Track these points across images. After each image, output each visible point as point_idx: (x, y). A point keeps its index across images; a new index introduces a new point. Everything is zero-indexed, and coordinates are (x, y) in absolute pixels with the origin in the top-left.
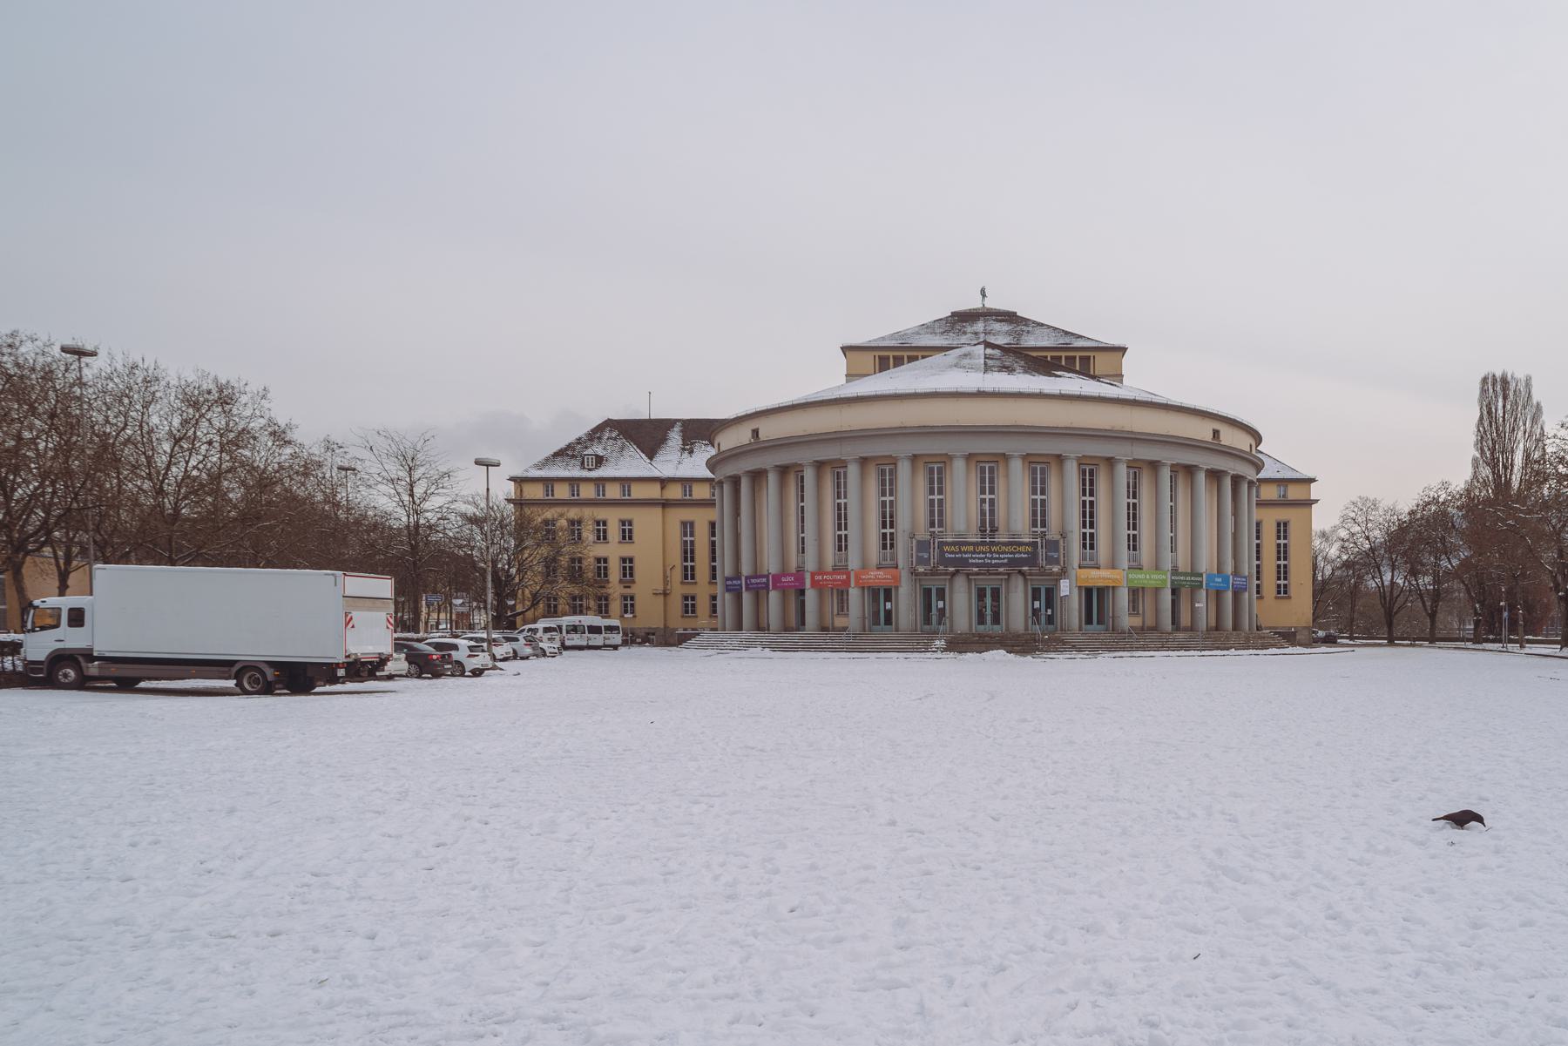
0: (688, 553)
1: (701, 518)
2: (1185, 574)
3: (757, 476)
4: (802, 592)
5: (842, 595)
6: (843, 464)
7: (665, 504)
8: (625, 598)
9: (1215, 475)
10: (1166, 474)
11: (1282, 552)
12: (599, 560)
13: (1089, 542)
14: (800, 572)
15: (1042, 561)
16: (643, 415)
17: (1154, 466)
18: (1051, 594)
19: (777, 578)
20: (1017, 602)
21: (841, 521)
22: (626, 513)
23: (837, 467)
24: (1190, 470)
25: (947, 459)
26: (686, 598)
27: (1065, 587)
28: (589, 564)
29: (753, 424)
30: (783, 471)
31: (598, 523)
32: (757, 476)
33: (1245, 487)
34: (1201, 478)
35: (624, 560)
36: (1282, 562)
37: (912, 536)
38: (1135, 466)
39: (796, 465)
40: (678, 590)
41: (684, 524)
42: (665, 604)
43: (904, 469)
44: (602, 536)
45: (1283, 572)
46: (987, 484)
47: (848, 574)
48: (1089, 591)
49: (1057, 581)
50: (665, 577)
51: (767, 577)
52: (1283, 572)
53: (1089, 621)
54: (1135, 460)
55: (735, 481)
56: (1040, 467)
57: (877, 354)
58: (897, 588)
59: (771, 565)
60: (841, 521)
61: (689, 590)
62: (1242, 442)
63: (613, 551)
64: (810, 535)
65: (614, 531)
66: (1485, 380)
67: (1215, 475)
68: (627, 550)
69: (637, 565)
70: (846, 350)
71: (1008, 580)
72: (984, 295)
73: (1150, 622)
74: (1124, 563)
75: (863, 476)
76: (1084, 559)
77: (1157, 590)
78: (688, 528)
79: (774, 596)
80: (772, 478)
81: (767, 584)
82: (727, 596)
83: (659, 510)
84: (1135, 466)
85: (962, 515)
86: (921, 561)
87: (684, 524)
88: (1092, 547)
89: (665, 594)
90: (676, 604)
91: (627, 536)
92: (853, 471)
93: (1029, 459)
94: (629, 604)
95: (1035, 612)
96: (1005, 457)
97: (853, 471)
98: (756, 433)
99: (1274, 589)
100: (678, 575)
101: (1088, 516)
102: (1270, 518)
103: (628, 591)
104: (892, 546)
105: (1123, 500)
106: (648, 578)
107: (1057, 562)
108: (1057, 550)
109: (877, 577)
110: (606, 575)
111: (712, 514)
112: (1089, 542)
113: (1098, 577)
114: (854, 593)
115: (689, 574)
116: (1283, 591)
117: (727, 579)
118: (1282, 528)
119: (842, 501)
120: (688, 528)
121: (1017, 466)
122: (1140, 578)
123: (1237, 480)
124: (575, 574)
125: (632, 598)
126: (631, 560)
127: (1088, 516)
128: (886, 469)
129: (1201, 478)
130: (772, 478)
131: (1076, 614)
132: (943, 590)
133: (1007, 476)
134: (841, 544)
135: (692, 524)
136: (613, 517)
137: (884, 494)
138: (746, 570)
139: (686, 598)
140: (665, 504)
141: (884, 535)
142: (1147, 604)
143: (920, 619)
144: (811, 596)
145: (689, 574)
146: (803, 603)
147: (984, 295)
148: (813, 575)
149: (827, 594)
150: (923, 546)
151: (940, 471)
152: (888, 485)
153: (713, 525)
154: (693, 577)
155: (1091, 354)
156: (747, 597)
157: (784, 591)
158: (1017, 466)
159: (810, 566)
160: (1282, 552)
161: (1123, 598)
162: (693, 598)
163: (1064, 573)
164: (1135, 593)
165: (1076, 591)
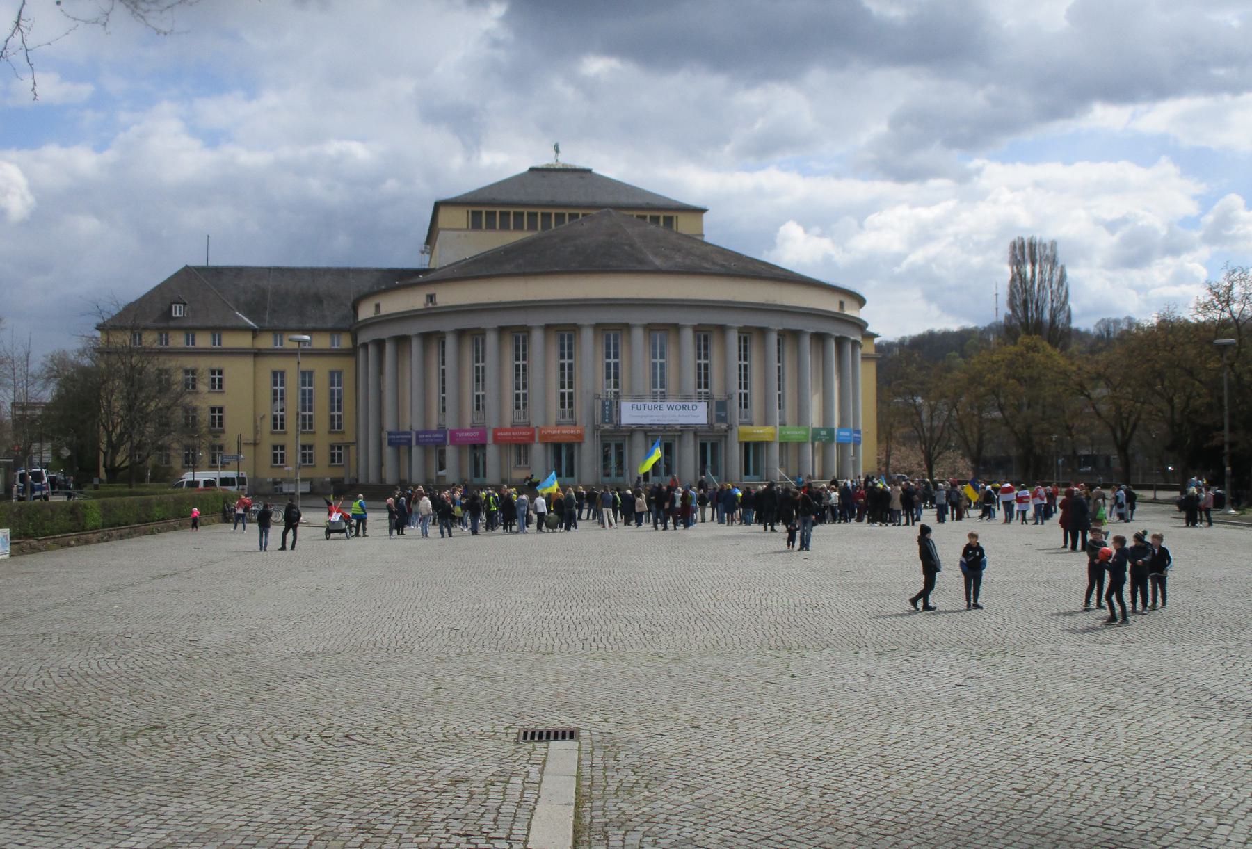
3: (402, 342)
7: (257, 354)
9: (820, 338)
10: (773, 338)
12: (213, 410)
13: (745, 401)
17: (763, 332)
19: (453, 433)
22: (216, 363)
23: (478, 335)
24: (796, 334)
25: (575, 329)
26: (275, 448)
28: (204, 416)
29: (430, 290)
30: (426, 337)
31: (213, 372)
32: (402, 342)
33: (849, 346)
34: (806, 342)
38: (746, 335)
39: (437, 333)
40: (268, 441)
41: (275, 374)
46: (612, 351)
48: (747, 445)
50: (256, 427)
53: (747, 473)
54: (745, 327)
56: (704, 335)
57: (471, 209)
58: (580, 444)
59: (413, 422)
61: (279, 440)
62: (829, 304)
63: (205, 400)
66: (1013, 246)
68: (216, 400)
71: (680, 436)
75: (500, 340)
76: (563, 416)
78: (278, 376)
80: (416, 345)
81: (410, 440)
84: (783, 334)
88: (746, 406)
90: (266, 452)
91: (217, 384)
92: (491, 339)
96: (627, 327)
97: (491, 339)
98: (431, 298)
100: (267, 425)
105: (734, 361)
106: (238, 425)
110: (221, 425)
113: (760, 432)
119: (480, 364)
120: (278, 376)
121: (688, 337)
123: (840, 342)
126: (221, 410)
128: (520, 335)
129: (806, 342)
130: (416, 345)
131: (738, 466)
133: (630, 343)
135: (282, 374)
136: (204, 364)
137: (517, 359)
138: (389, 426)
139: (275, 448)
140: (257, 354)
143: (600, 471)
144: (492, 452)
151: (570, 339)
152: (522, 351)
155: (674, 214)
158: (638, 335)
161: (775, 451)
164: (783, 445)
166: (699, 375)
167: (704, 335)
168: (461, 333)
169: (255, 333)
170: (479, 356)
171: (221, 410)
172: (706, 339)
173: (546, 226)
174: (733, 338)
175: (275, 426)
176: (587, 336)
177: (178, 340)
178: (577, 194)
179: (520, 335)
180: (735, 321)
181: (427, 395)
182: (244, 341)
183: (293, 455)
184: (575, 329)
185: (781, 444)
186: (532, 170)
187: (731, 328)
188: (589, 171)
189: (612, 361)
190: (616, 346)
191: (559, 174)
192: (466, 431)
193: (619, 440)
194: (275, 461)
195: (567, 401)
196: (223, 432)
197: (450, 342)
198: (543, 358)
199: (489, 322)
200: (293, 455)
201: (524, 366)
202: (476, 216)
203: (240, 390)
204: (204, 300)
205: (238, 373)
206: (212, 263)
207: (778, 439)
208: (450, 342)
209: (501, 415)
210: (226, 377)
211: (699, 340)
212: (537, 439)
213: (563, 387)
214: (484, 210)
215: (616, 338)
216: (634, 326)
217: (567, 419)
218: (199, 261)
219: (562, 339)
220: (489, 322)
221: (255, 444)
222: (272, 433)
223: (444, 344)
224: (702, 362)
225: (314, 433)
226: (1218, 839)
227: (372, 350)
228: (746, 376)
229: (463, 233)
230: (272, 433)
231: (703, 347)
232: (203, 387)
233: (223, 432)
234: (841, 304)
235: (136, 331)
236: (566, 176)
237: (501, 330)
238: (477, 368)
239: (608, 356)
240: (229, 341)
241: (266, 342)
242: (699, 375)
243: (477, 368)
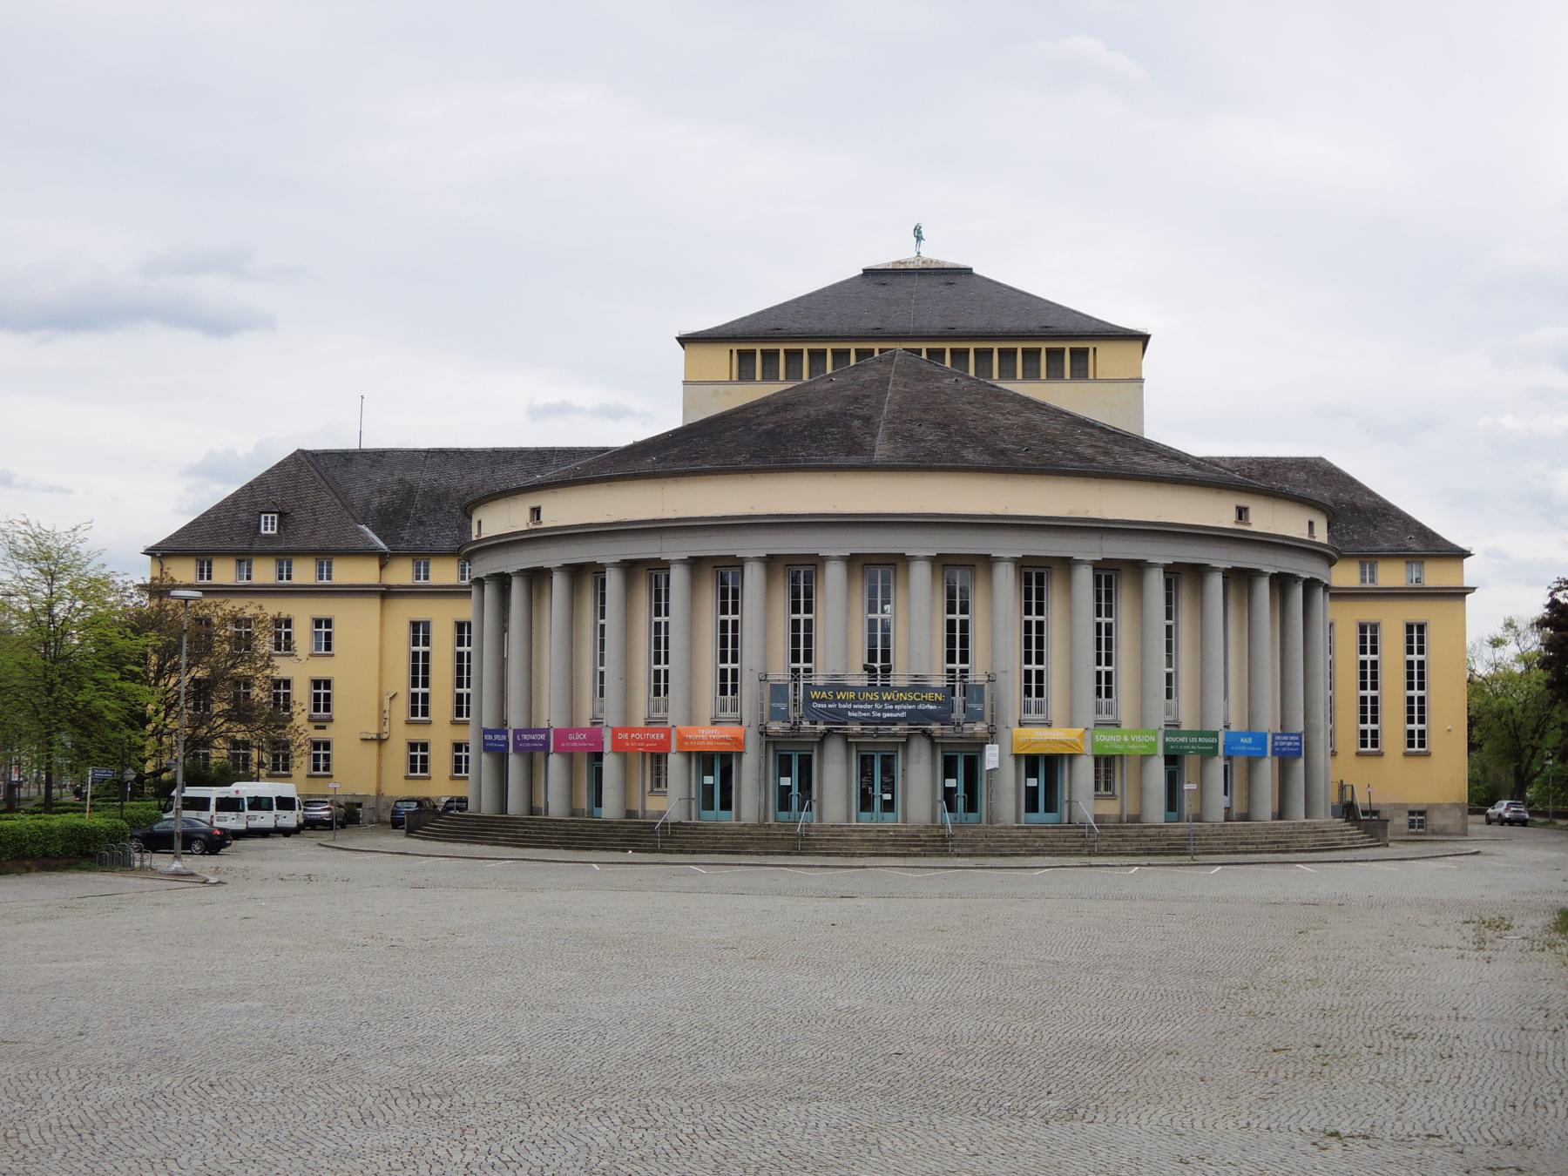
0: (420, 669)
1: (442, 617)
2: (1190, 734)
3: (537, 578)
4: (598, 757)
5: (658, 759)
6: (738, 564)
7: (386, 593)
8: (316, 745)
11: (1416, 675)
13: (1034, 685)
14: (595, 734)
15: (958, 715)
16: (351, 444)
17: (1138, 568)
18: (973, 764)
19: (561, 734)
20: (919, 780)
21: (660, 651)
22: (323, 607)
25: (815, 563)
27: (991, 756)
29: (1243, 501)
30: (576, 572)
35: (317, 684)
36: (1416, 693)
37: (764, 679)
38: (1108, 575)
40: (401, 735)
41: (415, 625)
42: (380, 756)
43: (753, 577)
44: (284, 644)
45: (1416, 710)
47: (668, 733)
49: (982, 746)
50: (382, 711)
51: (546, 731)
52: (1416, 710)
55: (502, 582)
57: (736, 347)
58: (740, 755)
59: (551, 715)
60: (660, 651)
61: (418, 735)
63: (299, 670)
64: (611, 668)
65: (302, 635)
67: (1240, 579)
68: (321, 669)
69: (337, 692)
70: (684, 340)
72: (919, 238)
73: (1131, 809)
74: (1089, 717)
76: (1027, 710)
77: (1144, 759)
78: (420, 631)
79: (556, 763)
80: (559, 582)
81: (546, 743)
82: (485, 757)
83: (374, 604)
84: (1173, 573)
85: (839, 653)
86: (776, 715)
87: (415, 625)
88: (1040, 693)
89: (380, 741)
90: (398, 755)
92: (678, 577)
93: (942, 563)
94: (321, 751)
95: (949, 794)
97: (678, 577)
99: (1404, 739)
100: (402, 708)
101: (1034, 643)
102: (1392, 620)
103: (320, 735)
104: (735, 690)
107: (979, 717)
108: (981, 700)
109: (708, 735)
111: (464, 610)
112: (1034, 685)
113: (1040, 739)
114: (675, 762)
115: (419, 706)
116: (1417, 740)
117: (486, 732)
118: (1416, 635)
120: (420, 631)
121: (920, 574)
122: (1110, 741)
124: (242, 711)
125: (327, 745)
126: (328, 684)
127: (1034, 643)
128: (723, 575)
130: (559, 582)
132: (809, 758)
133: (907, 586)
134: (660, 685)
135: (427, 624)
136: (302, 614)
138: (515, 721)
139: (413, 746)
140: (386, 593)
141: (724, 672)
142: (1123, 780)
144: (610, 764)
145: (419, 706)
146: (599, 771)
147: (919, 238)
148: (615, 732)
149: (636, 763)
150: (778, 691)
153: (461, 626)
154: (425, 712)
155: (1090, 345)
156: (514, 763)
157: (570, 759)
158: (920, 574)
159: (612, 718)
160: (1416, 675)
161: (1085, 772)
162: (425, 747)
163: (992, 736)
164: (1106, 765)
165: (1010, 762)
166: (735, 644)
167: (1035, 579)
168: (630, 568)
169: (384, 559)
170: (660, 605)
171: (328, 684)
172: (1040, 581)
173: (793, 372)
174: (1084, 579)
175: (414, 712)
176: (834, 577)
177: (264, 572)
178: (933, 312)
179: (723, 575)
180: (1162, 554)
181: (574, 671)
182: (363, 572)
183: (441, 759)
184: (815, 563)
185: (1097, 759)
186: (868, 273)
187: (1153, 565)
188: (967, 272)
189: (802, 616)
190: (1040, 596)
191: (903, 279)
192: (636, 730)
193: (887, 751)
194: (413, 769)
195: (728, 683)
196: (330, 720)
197: (613, 580)
198: (692, 617)
199: (673, 549)
200: (441, 759)
201: (735, 623)
202: (745, 358)
203: (356, 654)
204: (330, 508)
205: (356, 623)
206: (369, 444)
207: (1086, 748)
208: (613, 580)
209: (623, 706)
210: (337, 631)
211: (1028, 581)
212: (674, 748)
213: (1040, 674)
214: (758, 347)
215: (886, 580)
216: (913, 558)
217: (1369, 749)
218: (893, 251)
219: (795, 580)
220: (673, 549)
221: (380, 741)
222: (408, 723)
223: (603, 581)
224: (1034, 618)
225: (430, 723)
226: (548, 1173)
227: (489, 591)
228: (658, 645)
229: (721, 388)
230: (408, 723)
231: (1105, 599)
232: (265, 644)
233: (330, 720)
234: (1242, 513)
235: (204, 559)
236: (923, 283)
237: (770, 562)
238: (724, 623)
239: (796, 610)
240: (347, 572)
241: (401, 573)
242: (735, 644)
243: (658, 625)
